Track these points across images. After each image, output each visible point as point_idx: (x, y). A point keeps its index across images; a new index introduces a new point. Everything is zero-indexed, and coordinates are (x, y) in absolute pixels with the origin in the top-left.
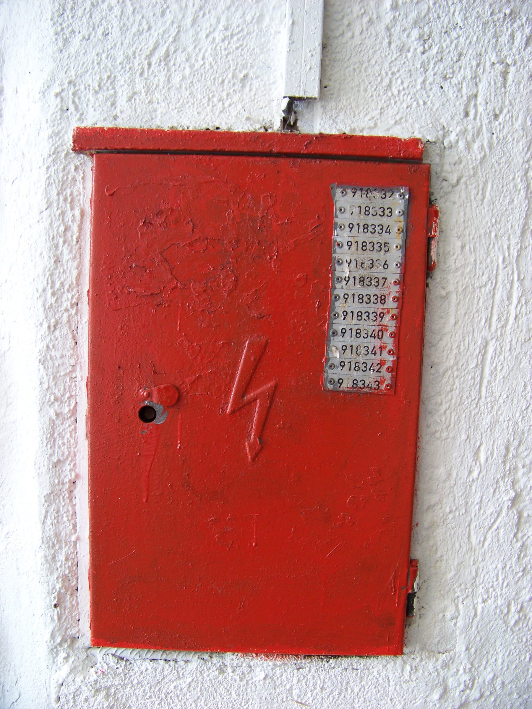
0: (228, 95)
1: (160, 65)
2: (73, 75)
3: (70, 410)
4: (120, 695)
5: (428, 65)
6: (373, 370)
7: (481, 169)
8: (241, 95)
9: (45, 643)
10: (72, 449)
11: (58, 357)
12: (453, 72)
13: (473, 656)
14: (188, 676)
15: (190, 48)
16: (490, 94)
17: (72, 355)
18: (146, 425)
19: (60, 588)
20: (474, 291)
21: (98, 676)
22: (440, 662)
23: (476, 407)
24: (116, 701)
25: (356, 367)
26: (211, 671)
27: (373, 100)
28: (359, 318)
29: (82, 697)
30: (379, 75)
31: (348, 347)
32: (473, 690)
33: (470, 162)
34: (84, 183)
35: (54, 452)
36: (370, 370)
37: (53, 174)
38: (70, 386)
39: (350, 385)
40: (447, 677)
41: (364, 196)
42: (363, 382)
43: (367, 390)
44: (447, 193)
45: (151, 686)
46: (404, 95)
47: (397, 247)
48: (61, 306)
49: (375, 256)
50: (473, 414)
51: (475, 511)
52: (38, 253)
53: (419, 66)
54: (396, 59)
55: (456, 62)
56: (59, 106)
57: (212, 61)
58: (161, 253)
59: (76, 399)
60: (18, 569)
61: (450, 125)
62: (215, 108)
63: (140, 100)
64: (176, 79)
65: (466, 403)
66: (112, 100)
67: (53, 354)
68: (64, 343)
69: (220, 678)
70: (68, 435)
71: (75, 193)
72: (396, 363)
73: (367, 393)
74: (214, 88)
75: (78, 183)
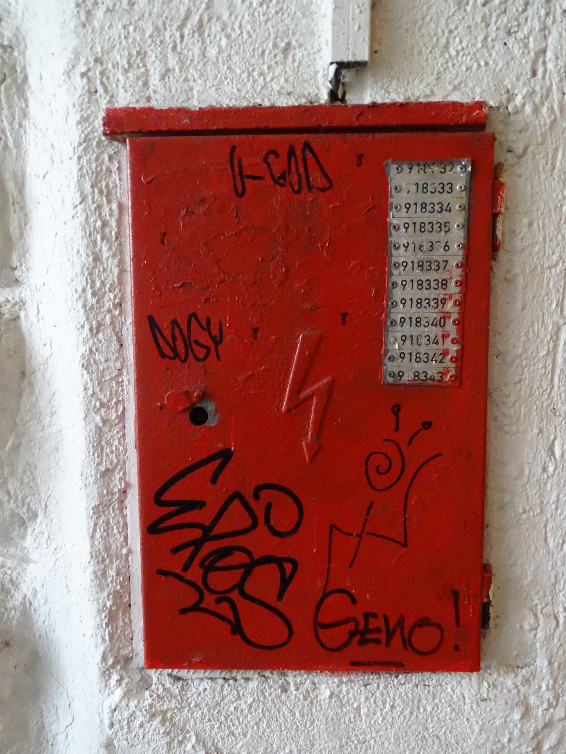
0: (269, 67)
1: (193, 37)
2: (99, 52)
3: (117, 416)
4: (177, 719)
5: (490, 19)
6: (436, 361)
7: (551, 134)
8: (284, 67)
9: (96, 665)
10: (121, 456)
11: (102, 360)
12: (519, 25)
13: (556, 672)
14: (249, 696)
15: (225, 16)
16: (562, 47)
17: (117, 358)
18: (198, 428)
19: (111, 606)
20: (543, 273)
21: (154, 700)
22: (520, 678)
23: (549, 398)
24: (173, 726)
25: (417, 358)
26: (273, 690)
27: (428, 64)
28: (419, 305)
29: (137, 723)
30: (435, 34)
31: (408, 337)
32: (557, 709)
33: (538, 128)
34: (120, 174)
35: (102, 460)
36: (432, 360)
37: (85, 164)
38: (117, 391)
39: (411, 377)
40: (529, 695)
41: (422, 172)
42: (425, 374)
43: (430, 382)
44: (512, 166)
45: (210, 708)
46: (463, 56)
47: (459, 226)
48: (103, 307)
49: (434, 237)
50: (545, 405)
51: (552, 511)
52: (75, 251)
53: (480, 21)
54: (453, 15)
55: (523, 12)
56: (87, 88)
57: (250, 29)
58: (205, 245)
59: (124, 404)
60: (67, 586)
61: (515, 86)
62: (256, 84)
63: (174, 77)
64: (212, 52)
65: (537, 393)
66: (143, 79)
67: (97, 357)
68: (108, 346)
69: (283, 697)
70: (116, 442)
71: (111, 185)
72: (461, 353)
73: (429, 386)
74: (253, 61)
75: (113, 175)
